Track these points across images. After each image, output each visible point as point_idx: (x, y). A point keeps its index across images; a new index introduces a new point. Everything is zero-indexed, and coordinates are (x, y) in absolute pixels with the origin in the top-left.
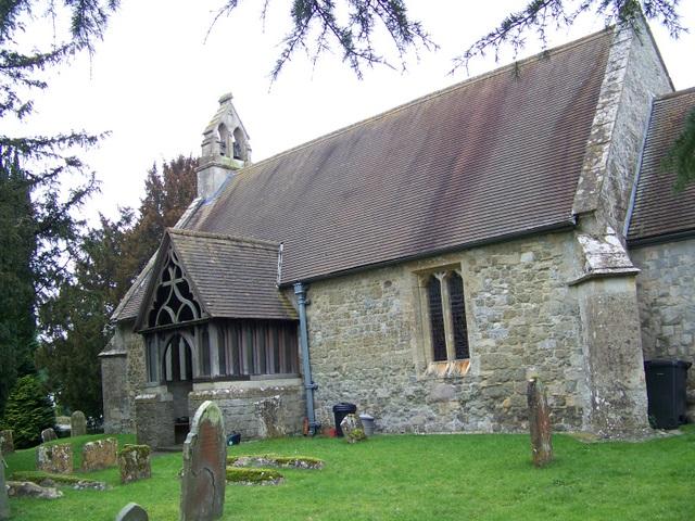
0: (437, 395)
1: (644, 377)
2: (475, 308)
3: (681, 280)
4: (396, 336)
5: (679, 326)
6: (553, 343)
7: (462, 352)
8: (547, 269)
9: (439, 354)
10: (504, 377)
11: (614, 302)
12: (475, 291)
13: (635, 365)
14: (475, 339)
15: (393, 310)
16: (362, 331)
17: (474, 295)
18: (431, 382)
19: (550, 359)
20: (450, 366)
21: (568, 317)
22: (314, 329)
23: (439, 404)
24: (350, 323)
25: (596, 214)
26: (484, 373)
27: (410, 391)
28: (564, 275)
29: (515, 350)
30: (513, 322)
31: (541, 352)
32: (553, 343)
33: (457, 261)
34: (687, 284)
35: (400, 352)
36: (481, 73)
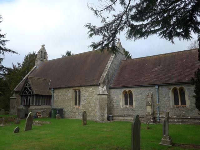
15: (69, 96)
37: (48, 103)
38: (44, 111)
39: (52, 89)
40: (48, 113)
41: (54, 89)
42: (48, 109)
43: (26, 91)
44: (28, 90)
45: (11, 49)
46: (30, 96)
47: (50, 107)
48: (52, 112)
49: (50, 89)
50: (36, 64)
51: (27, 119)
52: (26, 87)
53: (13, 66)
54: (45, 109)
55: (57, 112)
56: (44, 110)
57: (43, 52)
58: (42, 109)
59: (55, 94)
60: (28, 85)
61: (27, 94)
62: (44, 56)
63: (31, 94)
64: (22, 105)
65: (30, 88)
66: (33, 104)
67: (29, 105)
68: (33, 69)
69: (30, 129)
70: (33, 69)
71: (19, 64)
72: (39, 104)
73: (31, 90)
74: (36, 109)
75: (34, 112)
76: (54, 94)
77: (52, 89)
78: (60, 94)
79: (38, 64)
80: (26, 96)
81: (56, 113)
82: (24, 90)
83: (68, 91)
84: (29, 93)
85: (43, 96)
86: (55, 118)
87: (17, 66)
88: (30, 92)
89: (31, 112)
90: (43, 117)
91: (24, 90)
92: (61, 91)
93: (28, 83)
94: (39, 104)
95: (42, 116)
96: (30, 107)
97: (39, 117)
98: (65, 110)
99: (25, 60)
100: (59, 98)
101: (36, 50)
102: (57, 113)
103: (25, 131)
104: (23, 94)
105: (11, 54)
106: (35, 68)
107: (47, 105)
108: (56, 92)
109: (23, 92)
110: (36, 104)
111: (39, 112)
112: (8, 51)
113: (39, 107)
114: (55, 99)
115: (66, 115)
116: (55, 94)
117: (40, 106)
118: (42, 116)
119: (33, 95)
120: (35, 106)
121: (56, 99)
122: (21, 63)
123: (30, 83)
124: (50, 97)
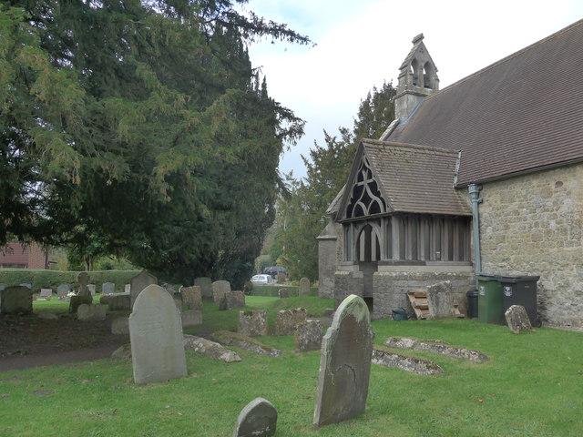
15: (564, 209)
24: (520, 219)
37: (456, 252)
38: (439, 288)
39: (472, 189)
40: (460, 296)
41: (481, 185)
42: (458, 277)
43: (359, 202)
44: (366, 200)
45: (279, 22)
46: (378, 220)
47: (467, 269)
48: (482, 293)
49: (461, 188)
50: (397, 110)
51: (325, 345)
52: (360, 184)
53: (328, 139)
54: (445, 277)
55: (508, 294)
56: (442, 283)
57: (419, 64)
58: (434, 277)
59: (485, 210)
60: (365, 174)
61: (366, 212)
62: (427, 78)
63: (379, 216)
64: (349, 263)
65: (373, 186)
66: (389, 255)
67: (375, 266)
68: (388, 131)
69: (356, 413)
70: (388, 131)
71: (344, 131)
72: (415, 254)
73: (377, 194)
74: (406, 278)
75: (397, 290)
76: (481, 210)
77: (472, 189)
78: (514, 206)
79: (405, 111)
80: (360, 222)
81: (502, 303)
82: (354, 201)
83: (559, 184)
84: (371, 212)
85: (430, 218)
86: (501, 320)
87: (339, 139)
88: (375, 202)
89: (352, 297)
90: (437, 317)
91: (354, 201)
92: (518, 189)
93: (365, 168)
94: (415, 254)
95: (431, 312)
96: (380, 268)
97: (418, 313)
98: (548, 284)
99: (360, 115)
100: (507, 227)
101: (387, 72)
102: (511, 301)
103: (322, 424)
104: (349, 215)
105: (283, 41)
106: (396, 126)
107: (451, 258)
108: (493, 196)
109: (350, 208)
110: (402, 254)
111: (420, 290)
112: (267, 30)
113: (419, 270)
114: (489, 232)
115: (552, 311)
116: (485, 210)
117: (423, 264)
118: (431, 312)
119: (388, 218)
120: (397, 264)
121: (494, 230)
122: (351, 128)
123: (374, 165)
124: (463, 222)
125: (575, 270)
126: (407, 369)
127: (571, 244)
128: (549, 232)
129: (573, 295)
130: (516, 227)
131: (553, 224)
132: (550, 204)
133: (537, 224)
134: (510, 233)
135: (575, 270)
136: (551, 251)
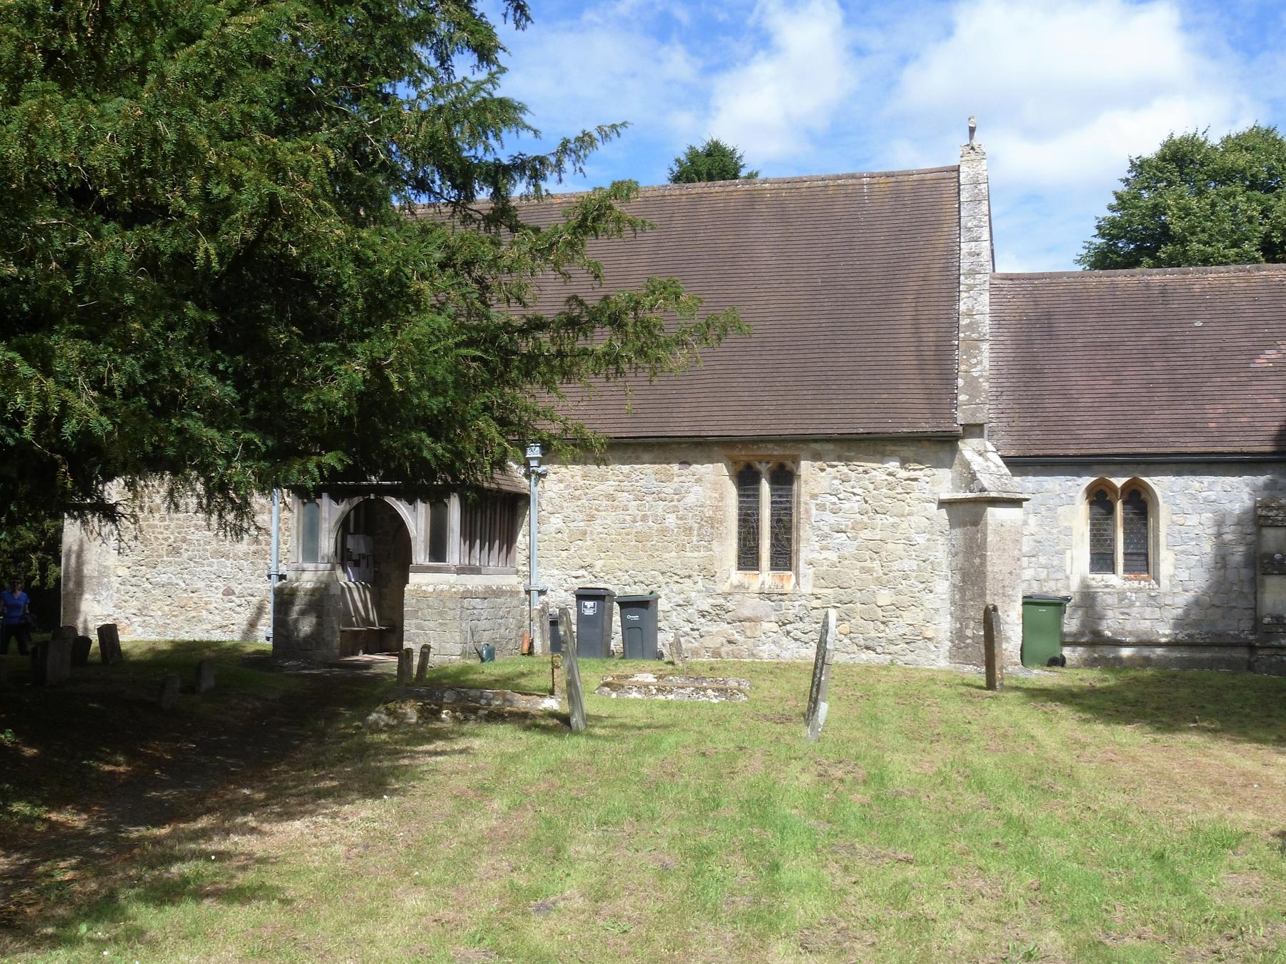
0: (746, 613)
1: (1021, 612)
2: (814, 512)
3: (1043, 508)
4: (690, 534)
5: (1033, 559)
6: (914, 564)
7: (783, 558)
8: (915, 480)
9: (748, 559)
10: (846, 599)
11: (1003, 529)
12: (816, 491)
13: (1013, 598)
14: (807, 548)
15: (691, 499)
16: (635, 521)
17: (814, 497)
18: (738, 597)
19: (908, 583)
20: (765, 577)
21: (935, 537)
22: (550, 509)
23: (747, 624)
24: (615, 508)
25: (229, 13)
26: (817, 591)
27: (705, 605)
28: (936, 489)
29: (863, 568)
30: (865, 534)
31: (897, 574)
32: (914, 564)
33: (792, 452)
34: (1048, 514)
35: (691, 554)
36: (815, 173)
100: (591, 518)
125: (700, 583)
126: (715, 701)
127: (697, 549)
128: (663, 532)
129: (696, 616)
130: (607, 518)
131: (671, 520)
132: (669, 489)
133: (644, 518)
134: (597, 526)
135: (700, 583)
136: (666, 555)
